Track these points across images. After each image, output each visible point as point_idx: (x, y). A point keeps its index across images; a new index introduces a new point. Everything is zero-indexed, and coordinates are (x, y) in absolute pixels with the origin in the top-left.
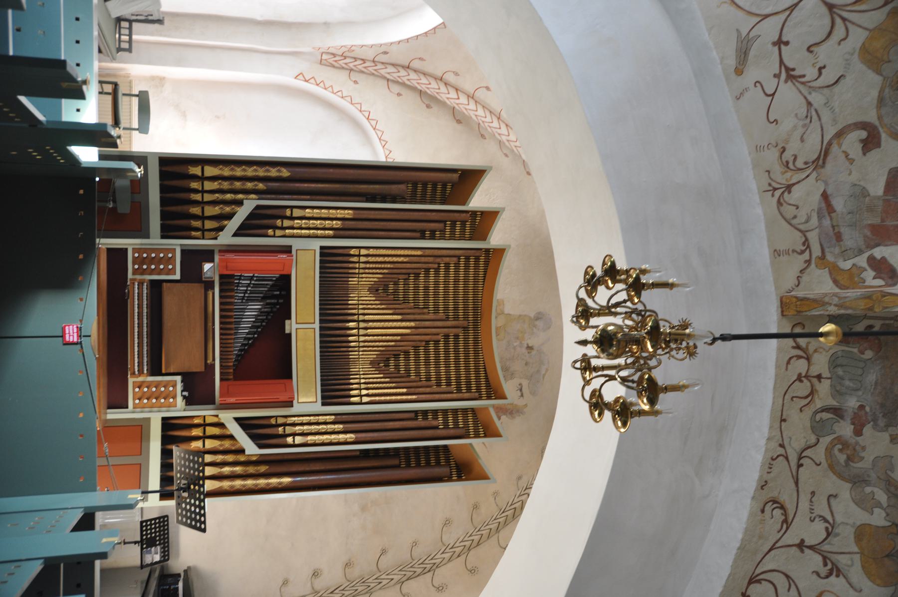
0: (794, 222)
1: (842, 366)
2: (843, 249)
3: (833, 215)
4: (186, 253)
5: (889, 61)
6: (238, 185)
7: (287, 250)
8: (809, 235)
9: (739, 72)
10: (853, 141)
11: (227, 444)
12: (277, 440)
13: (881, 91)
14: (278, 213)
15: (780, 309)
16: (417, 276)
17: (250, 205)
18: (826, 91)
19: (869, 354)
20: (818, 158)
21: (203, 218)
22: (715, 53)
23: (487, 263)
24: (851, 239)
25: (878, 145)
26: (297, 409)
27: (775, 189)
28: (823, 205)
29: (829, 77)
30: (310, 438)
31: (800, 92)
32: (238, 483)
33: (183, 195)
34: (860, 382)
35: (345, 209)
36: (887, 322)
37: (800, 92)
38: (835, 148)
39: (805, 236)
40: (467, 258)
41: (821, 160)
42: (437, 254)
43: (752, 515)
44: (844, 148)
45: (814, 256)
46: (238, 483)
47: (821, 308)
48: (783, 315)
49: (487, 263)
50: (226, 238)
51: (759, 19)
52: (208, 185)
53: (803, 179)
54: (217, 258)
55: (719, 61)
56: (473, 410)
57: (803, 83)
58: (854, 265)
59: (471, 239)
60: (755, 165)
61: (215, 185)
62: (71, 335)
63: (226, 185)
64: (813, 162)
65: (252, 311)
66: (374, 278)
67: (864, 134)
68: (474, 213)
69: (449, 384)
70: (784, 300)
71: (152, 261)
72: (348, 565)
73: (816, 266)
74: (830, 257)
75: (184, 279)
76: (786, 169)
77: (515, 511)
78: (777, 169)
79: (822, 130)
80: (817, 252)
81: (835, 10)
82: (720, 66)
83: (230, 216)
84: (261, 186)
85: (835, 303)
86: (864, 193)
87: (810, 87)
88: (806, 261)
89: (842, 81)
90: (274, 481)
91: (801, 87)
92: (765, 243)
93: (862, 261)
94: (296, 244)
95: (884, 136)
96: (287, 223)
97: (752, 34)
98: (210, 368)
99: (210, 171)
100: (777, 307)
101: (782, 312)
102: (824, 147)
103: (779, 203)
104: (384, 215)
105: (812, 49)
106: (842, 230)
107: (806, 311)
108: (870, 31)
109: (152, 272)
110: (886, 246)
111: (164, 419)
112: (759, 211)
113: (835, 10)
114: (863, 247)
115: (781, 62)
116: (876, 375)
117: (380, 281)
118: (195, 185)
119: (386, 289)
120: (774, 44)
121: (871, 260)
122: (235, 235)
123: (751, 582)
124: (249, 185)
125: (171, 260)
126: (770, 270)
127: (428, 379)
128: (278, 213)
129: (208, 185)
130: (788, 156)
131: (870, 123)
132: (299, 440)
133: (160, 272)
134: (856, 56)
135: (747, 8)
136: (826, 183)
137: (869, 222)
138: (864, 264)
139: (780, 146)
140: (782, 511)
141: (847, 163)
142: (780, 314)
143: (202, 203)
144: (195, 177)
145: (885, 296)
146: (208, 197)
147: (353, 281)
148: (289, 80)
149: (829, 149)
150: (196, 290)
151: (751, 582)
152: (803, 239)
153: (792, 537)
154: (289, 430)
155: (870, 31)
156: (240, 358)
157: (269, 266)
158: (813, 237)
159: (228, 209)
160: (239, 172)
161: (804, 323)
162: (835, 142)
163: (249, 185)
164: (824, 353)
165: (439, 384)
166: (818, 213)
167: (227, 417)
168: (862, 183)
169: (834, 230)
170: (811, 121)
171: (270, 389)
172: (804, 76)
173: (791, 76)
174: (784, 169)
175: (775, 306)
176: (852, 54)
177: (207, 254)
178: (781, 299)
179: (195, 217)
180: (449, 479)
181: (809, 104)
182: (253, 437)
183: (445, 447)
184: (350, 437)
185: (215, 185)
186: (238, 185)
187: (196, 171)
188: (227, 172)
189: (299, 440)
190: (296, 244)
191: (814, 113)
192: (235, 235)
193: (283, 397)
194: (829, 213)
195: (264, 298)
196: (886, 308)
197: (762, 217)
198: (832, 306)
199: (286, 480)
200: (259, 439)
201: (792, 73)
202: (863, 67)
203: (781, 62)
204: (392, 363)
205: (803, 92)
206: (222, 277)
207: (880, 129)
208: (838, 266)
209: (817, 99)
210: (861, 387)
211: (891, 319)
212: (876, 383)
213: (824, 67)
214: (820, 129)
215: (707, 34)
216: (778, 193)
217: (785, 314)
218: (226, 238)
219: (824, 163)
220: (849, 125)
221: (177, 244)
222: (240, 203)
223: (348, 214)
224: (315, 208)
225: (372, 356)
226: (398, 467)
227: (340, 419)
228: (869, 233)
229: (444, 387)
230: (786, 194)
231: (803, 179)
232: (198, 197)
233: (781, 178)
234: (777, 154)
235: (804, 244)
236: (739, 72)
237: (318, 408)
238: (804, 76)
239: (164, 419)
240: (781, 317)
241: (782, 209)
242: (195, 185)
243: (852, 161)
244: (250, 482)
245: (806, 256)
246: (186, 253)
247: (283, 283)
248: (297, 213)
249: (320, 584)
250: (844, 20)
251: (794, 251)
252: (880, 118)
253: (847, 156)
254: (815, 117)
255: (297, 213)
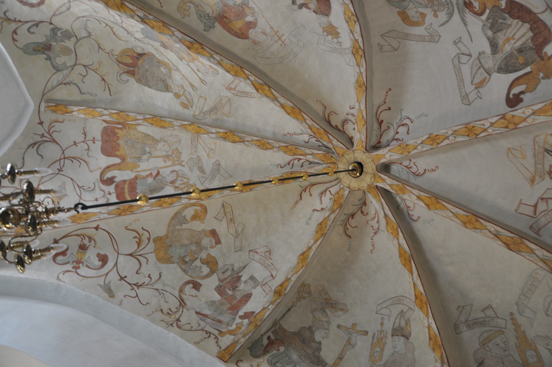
0: (193, 329)
1: (277, 362)
2: (226, 324)
3: (209, 317)
5: (172, 257)
8: (205, 329)
10: (189, 289)
13: (181, 268)
15: (222, 361)
18: (159, 281)
19: (282, 349)
20: (180, 303)
22: (93, 296)
24: (225, 318)
25: (201, 285)
27: (172, 324)
28: (201, 316)
29: (155, 277)
31: (148, 288)
34: (292, 362)
36: (272, 330)
37: (148, 288)
38: (184, 297)
39: (204, 331)
41: (182, 303)
44: (188, 294)
45: (216, 334)
47: (238, 344)
48: (225, 362)
51: (104, 277)
53: (182, 314)
55: (98, 297)
57: (146, 285)
58: (236, 324)
64: (180, 306)
67: (191, 285)
70: (219, 356)
73: (221, 337)
74: (223, 330)
76: (169, 315)
77: (13, 21)
78: (166, 318)
79: (172, 294)
80: (216, 333)
81: (133, 255)
82: (100, 299)
85: (240, 337)
86: (213, 302)
87: (151, 284)
88: (215, 338)
89: (162, 275)
91: (147, 286)
92: (187, 344)
93: (238, 320)
95: (199, 281)
97: (106, 282)
100: (219, 361)
101: (224, 361)
102: (179, 300)
105: (138, 272)
106: (218, 318)
107: (233, 351)
108: (154, 252)
110: (241, 309)
112: (172, 335)
113: (133, 255)
114: (233, 317)
115: (130, 284)
116: (295, 354)
120: (120, 280)
121: (241, 317)
126: (200, 351)
131: (189, 281)
134: (158, 263)
135: (95, 276)
136: (193, 309)
137: (226, 308)
138: (240, 321)
139: (159, 309)
140: (84, 136)
141: (195, 298)
142: (224, 363)
145: (256, 317)
149: (182, 299)
152: (205, 332)
155: (154, 252)
158: (208, 328)
161: (240, 359)
162: (182, 295)
164: (263, 363)
166: (201, 320)
168: (209, 300)
169: (215, 321)
170: (164, 294)
172: (145, 282)
173: (138, 286)
174: (169, 316)
175: (218, 362)
176: (156, 264)
178: (218, 357)
181: (157, 290)
191: (162, 291)
194: (206, 317)
196: (262, 320)
197: (175, 335)
198: (241, 339)
201: (138, 284)
202: (165, 265)
203: (130, 284)
205: (149, 287)
207: (195, 280)
208: (230, 330)
209: (158, 286)
210: (295, 363)
211: (272, 327)
212: (299, 357)
213: (150, 275)
214: (171, 294)
215: (83, 292)
216: (175, 325)
217: (225, 361)
219: (185, 303)
220: (182, 286)
228: (230, 311)
230: (179, 323)
231: (182, 314)
233: (172, 319)
234: (161, 313)
235: (207, 333)
238: (145, 282)
240: (225, 363)
241: (182, 328)
243: (196, 296)
245: (212, 336)
250: (140, 255)
251: (205, 338)
252: (191, 276)
253: (192, 296)
254: (164, 292)
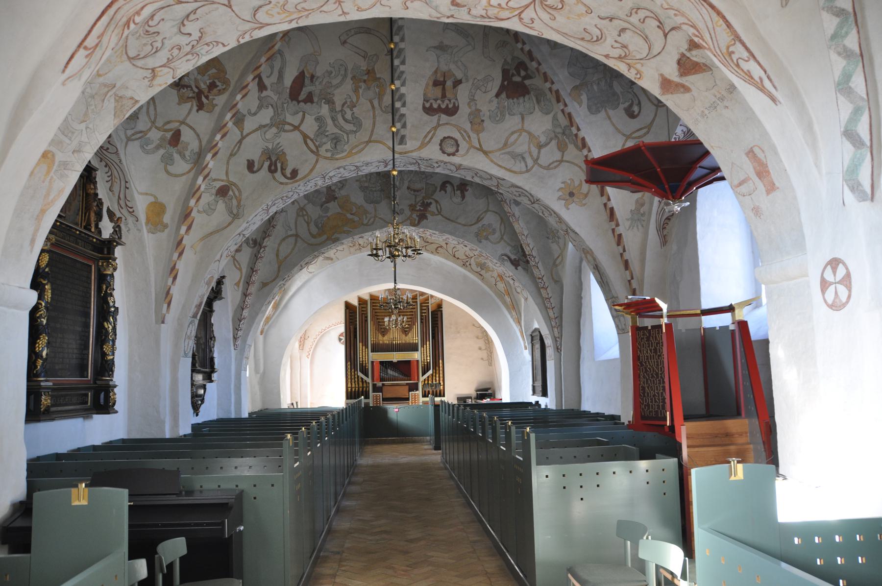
4: (374, 392)
6: (353, 377)
7: (372, 362)
9: (332, 259)
11: (430, 379)
12: (428, 364)
14: (362, 365)
16: (379, 322)
17: (360, 374)
21: (363, 387)
23: (374, 300)
26: (419, 359)
30: (428, 355)
32: (441, 375)
33: (356, 393)
35: (360, 345)
40: (373, 306)
42: (372, 317)
43: (439, 256)
46: (441, 375)
49: (374, 300)
50: (369, 380)
52: (353, 386)
54: (375, 383)
56: (421, 304)
59: (367, 305)
60: (354, 254)
61: (353, 384)
62: (397, 410)
63: (353, 381)
65: (390, 372)
66: (380, 336)
68: (359, 304)
69: (412, 312)
71: (376, 401)
72: (477, 338)
75: (381, 392)
78: (355, 247)
83: (362, 379)
84: (353, 370)
90: (441, 365)
94: (370, 360)
96: (364, 363)
98: (407, 384)
99: (349, 385)
103: (363, 247)
104: (361, 333)
109: (380, 401)
111: (423, 397)
117: (381, 334)
118: (353, 390)
119: (383, 332)
122: (368, 377)
123: (455, 257)
124: (353, 374)
125: (376, 395)
127: (411, 318)
128: (362, 365)
129: (353, 386)
130: (352, 245)
132: (428, 358)
133: (380, 398)
143: (359, 388)
144: (351, 390)
146: (357, 386)
147: (381, 342)
148: (309, 360)
150: (385, 389)
151: (455, 257)
153: (445, 246)
154: (425, 361)
156: (405, 375)
157: (377, 368)
159: (360, 380)
160: (349, 377)
163: (353, 374)
165: (413, 315)
167: (422, 379)
171: (414, 366)
177: (374, 386)
179: (363, 389)
180: (442, 311)
182: (428, 371)
183: (431, 312)
184: (428, 343)
185: (353, 384)
186: (353, 377)
187: (349, 389)
188: (350, 380)
189: (428, 358)
190: (370, 360)
192: (368, 377)
193: (416, 363)
195: (387, 369)
199: (441, 361)
200: (428, 370)
204: (406, 330)
206: (381, 381)
218: (369, 380)
221: (371, 394)
222: (358, 376)
223: (361, 344)
224: (360, 355)
225: (404, 336)
226: (438, 327)
227: (422, 346)
229: (414, 313)
232: (357, 389)
233: (358, 246)
236: (332, 259)
237: (419, 352)
239: (423, 397)
242: (353, 390)
244: (441, 372)
246: (374, 392)
247: (382, 363)
248: (361, 360)
249: (483, 348)
255: (361, 360)
